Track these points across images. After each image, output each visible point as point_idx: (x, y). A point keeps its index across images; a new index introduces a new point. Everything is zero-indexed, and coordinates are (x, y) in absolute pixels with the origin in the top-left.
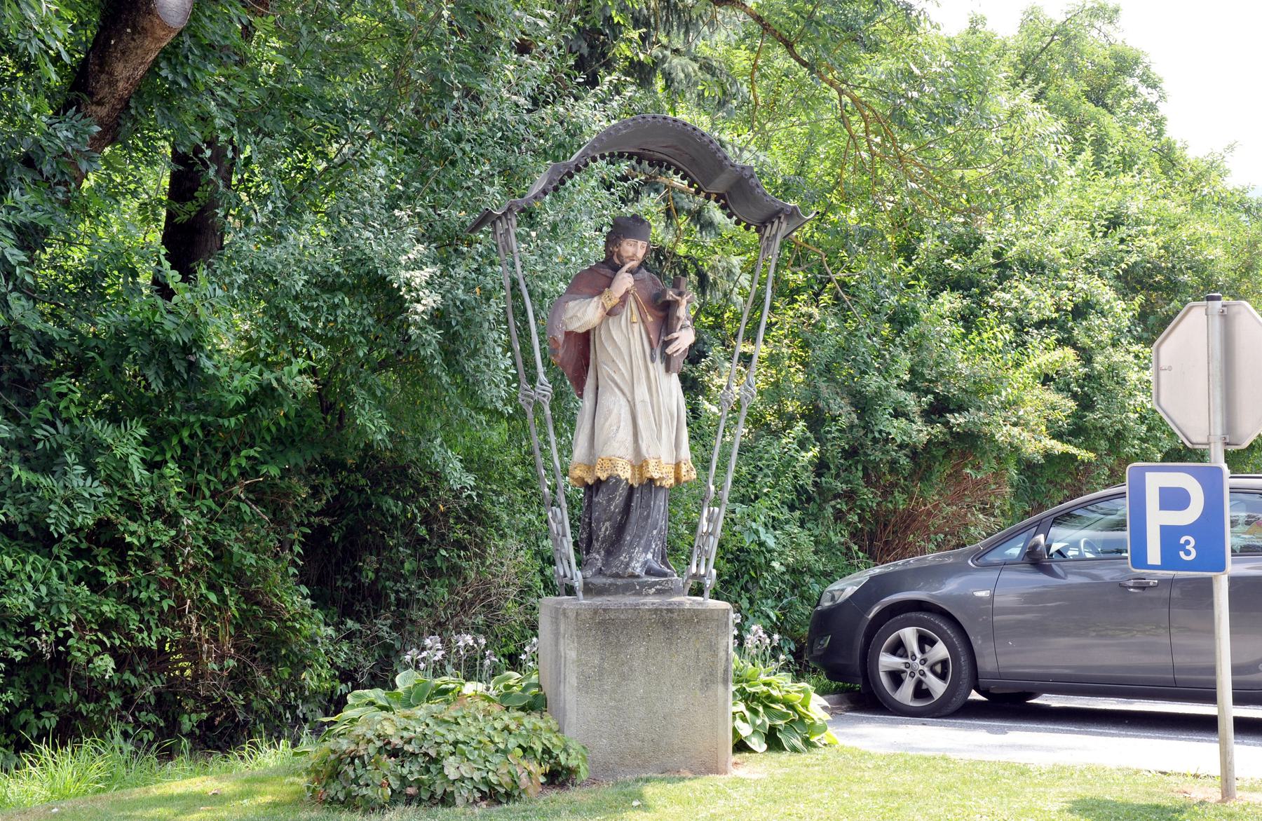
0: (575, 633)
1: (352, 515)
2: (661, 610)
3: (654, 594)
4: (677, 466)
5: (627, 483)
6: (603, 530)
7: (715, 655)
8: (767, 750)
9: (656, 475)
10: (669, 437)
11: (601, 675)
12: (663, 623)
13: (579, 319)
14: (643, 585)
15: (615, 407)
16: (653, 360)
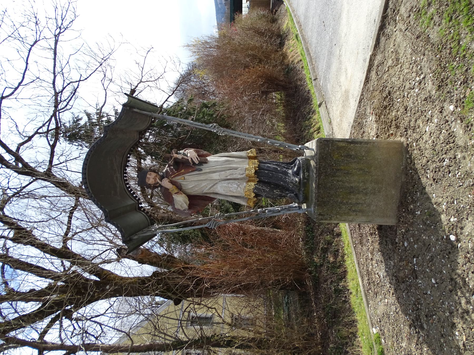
4: (250, 158)
5: (257, 184)
6: (277, 193)
9: (253, 171)
10: (237, 163)
15: (221, 188)
16: (201, 170)
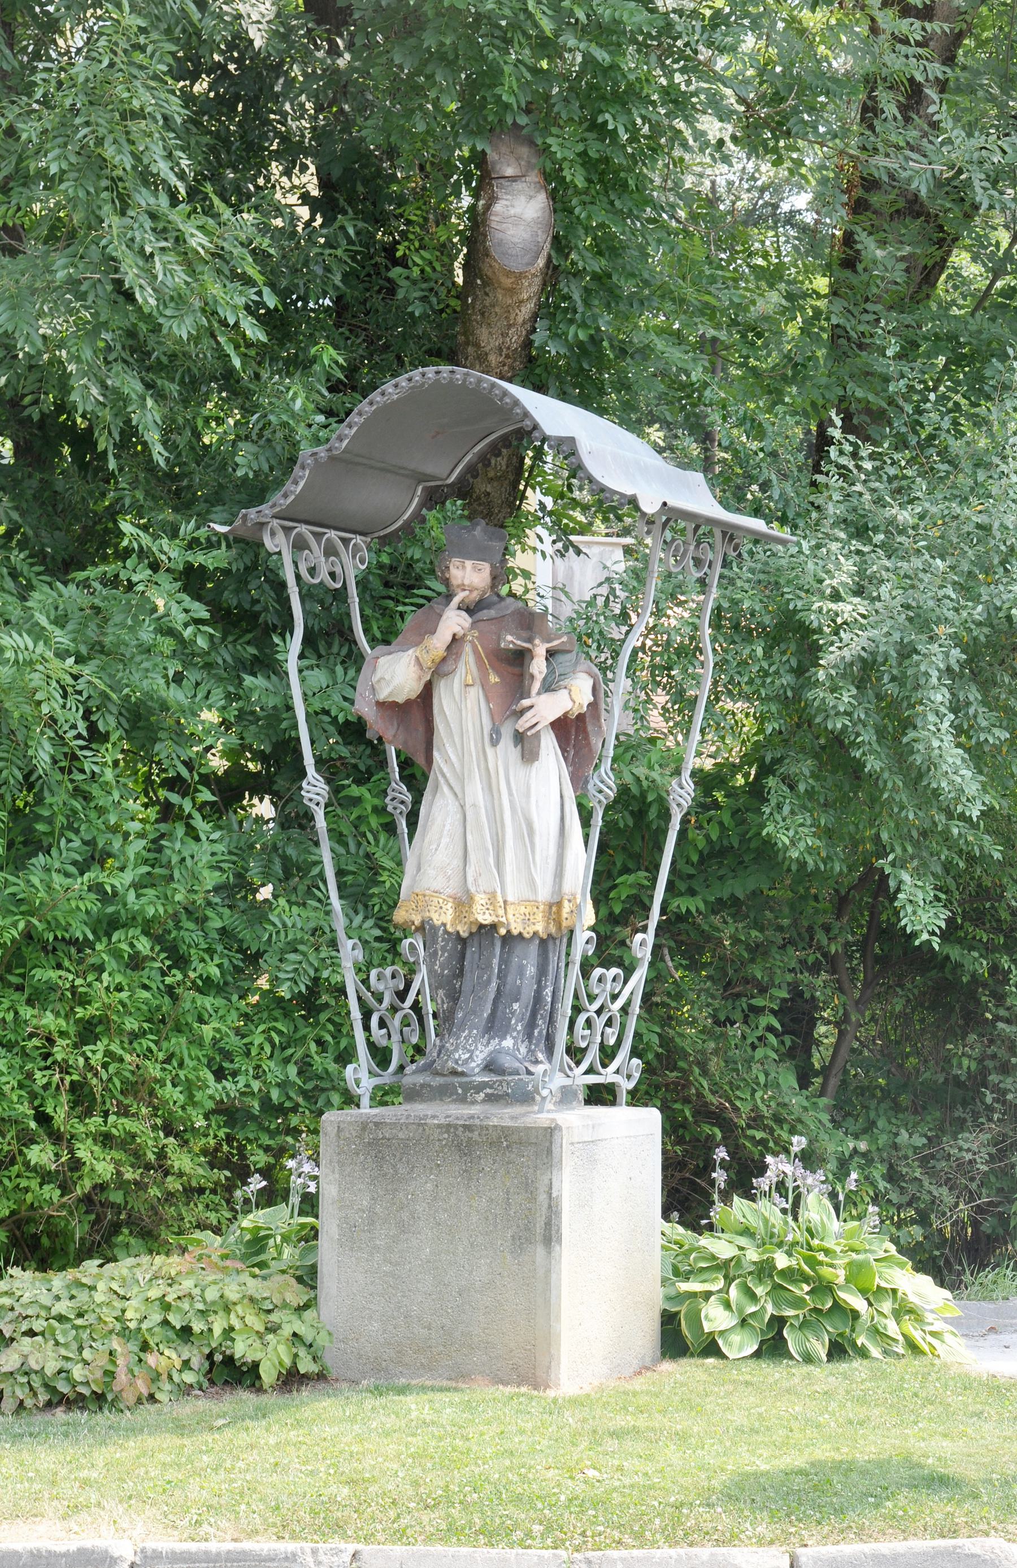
0: (336, 1158)
1: (934, 972)
2: (456, 1127)
3: (484, 1101)
7: (533, 1199)
8: (757, 1355)
11: (372, 1223)
12: (459, 1146)
13: (388, 684)
14: (467, 1087)
